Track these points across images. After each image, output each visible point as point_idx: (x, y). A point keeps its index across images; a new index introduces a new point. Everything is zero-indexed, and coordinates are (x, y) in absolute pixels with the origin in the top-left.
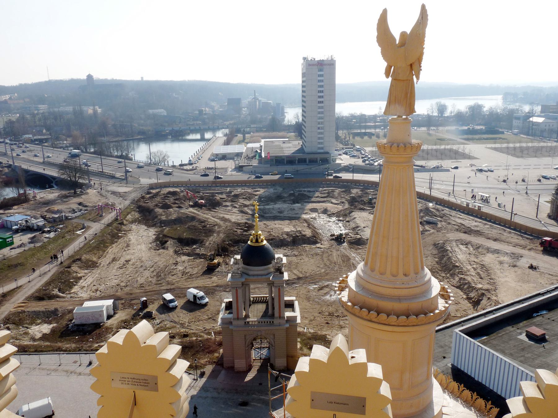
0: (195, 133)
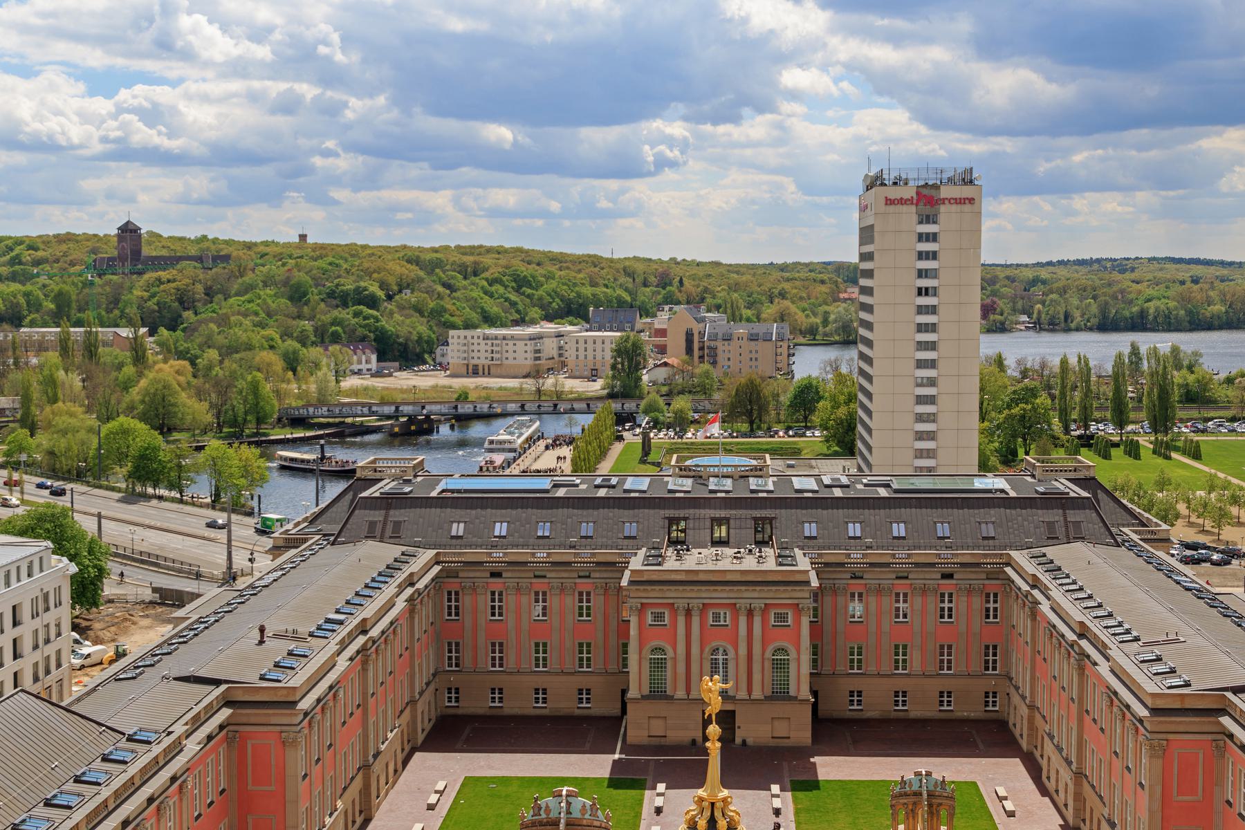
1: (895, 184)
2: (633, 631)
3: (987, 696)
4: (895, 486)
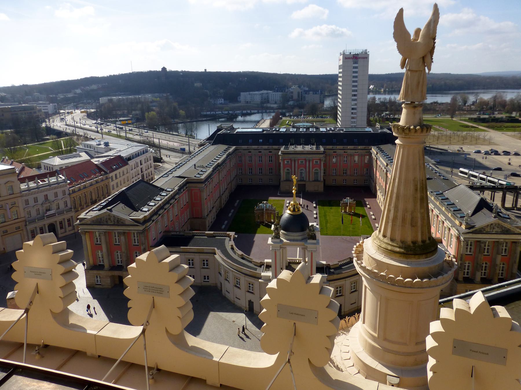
0: (108, 77)
3: (270, 180)
4: (344, 130)
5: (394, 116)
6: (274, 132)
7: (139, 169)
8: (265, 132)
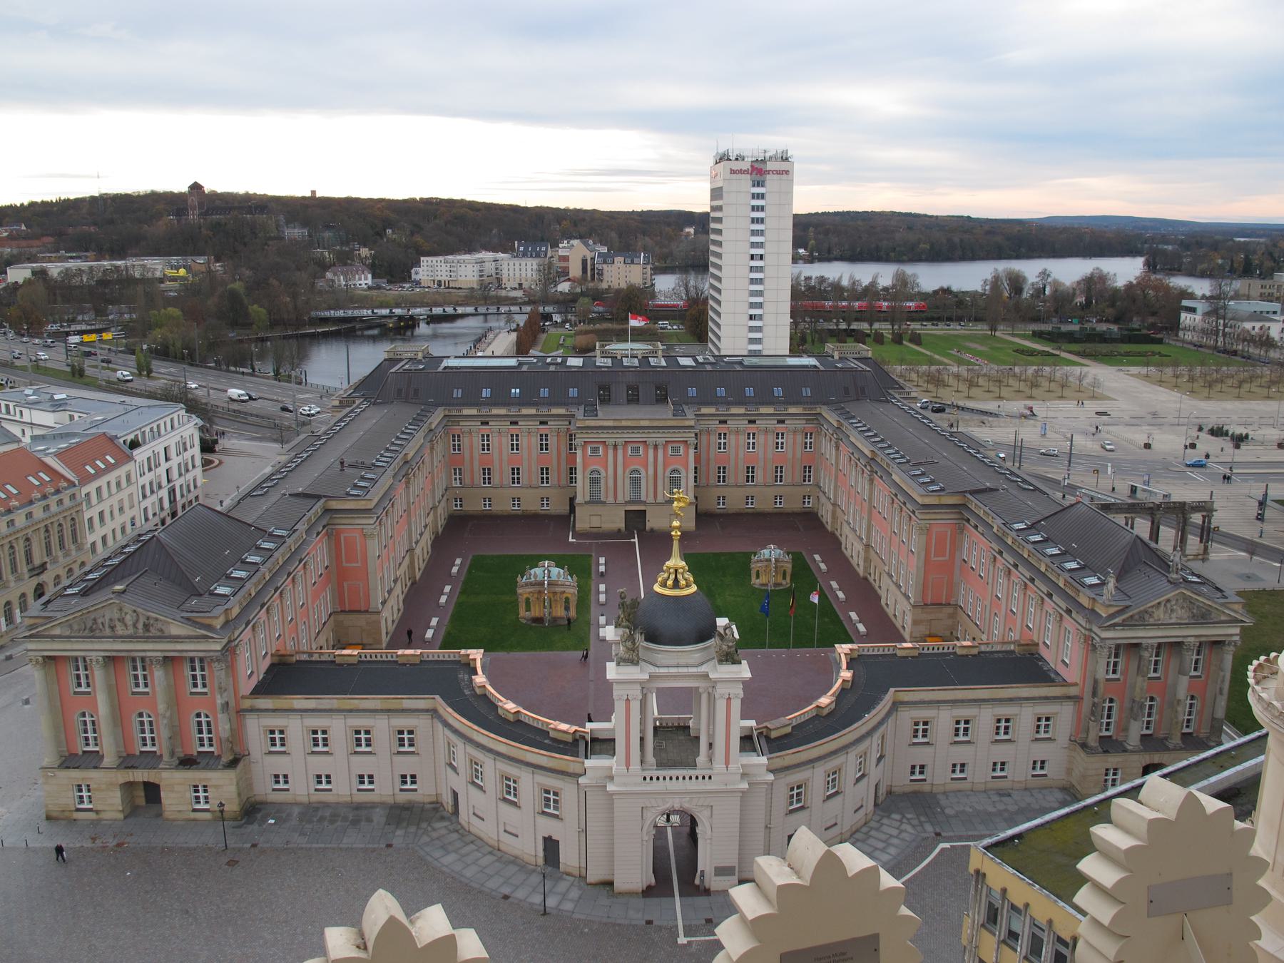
1: (737, 159)
2: (579, 460)
5: (849, 326)
6: (552, 368)
7: (161, 471)
8: (525, 368)
